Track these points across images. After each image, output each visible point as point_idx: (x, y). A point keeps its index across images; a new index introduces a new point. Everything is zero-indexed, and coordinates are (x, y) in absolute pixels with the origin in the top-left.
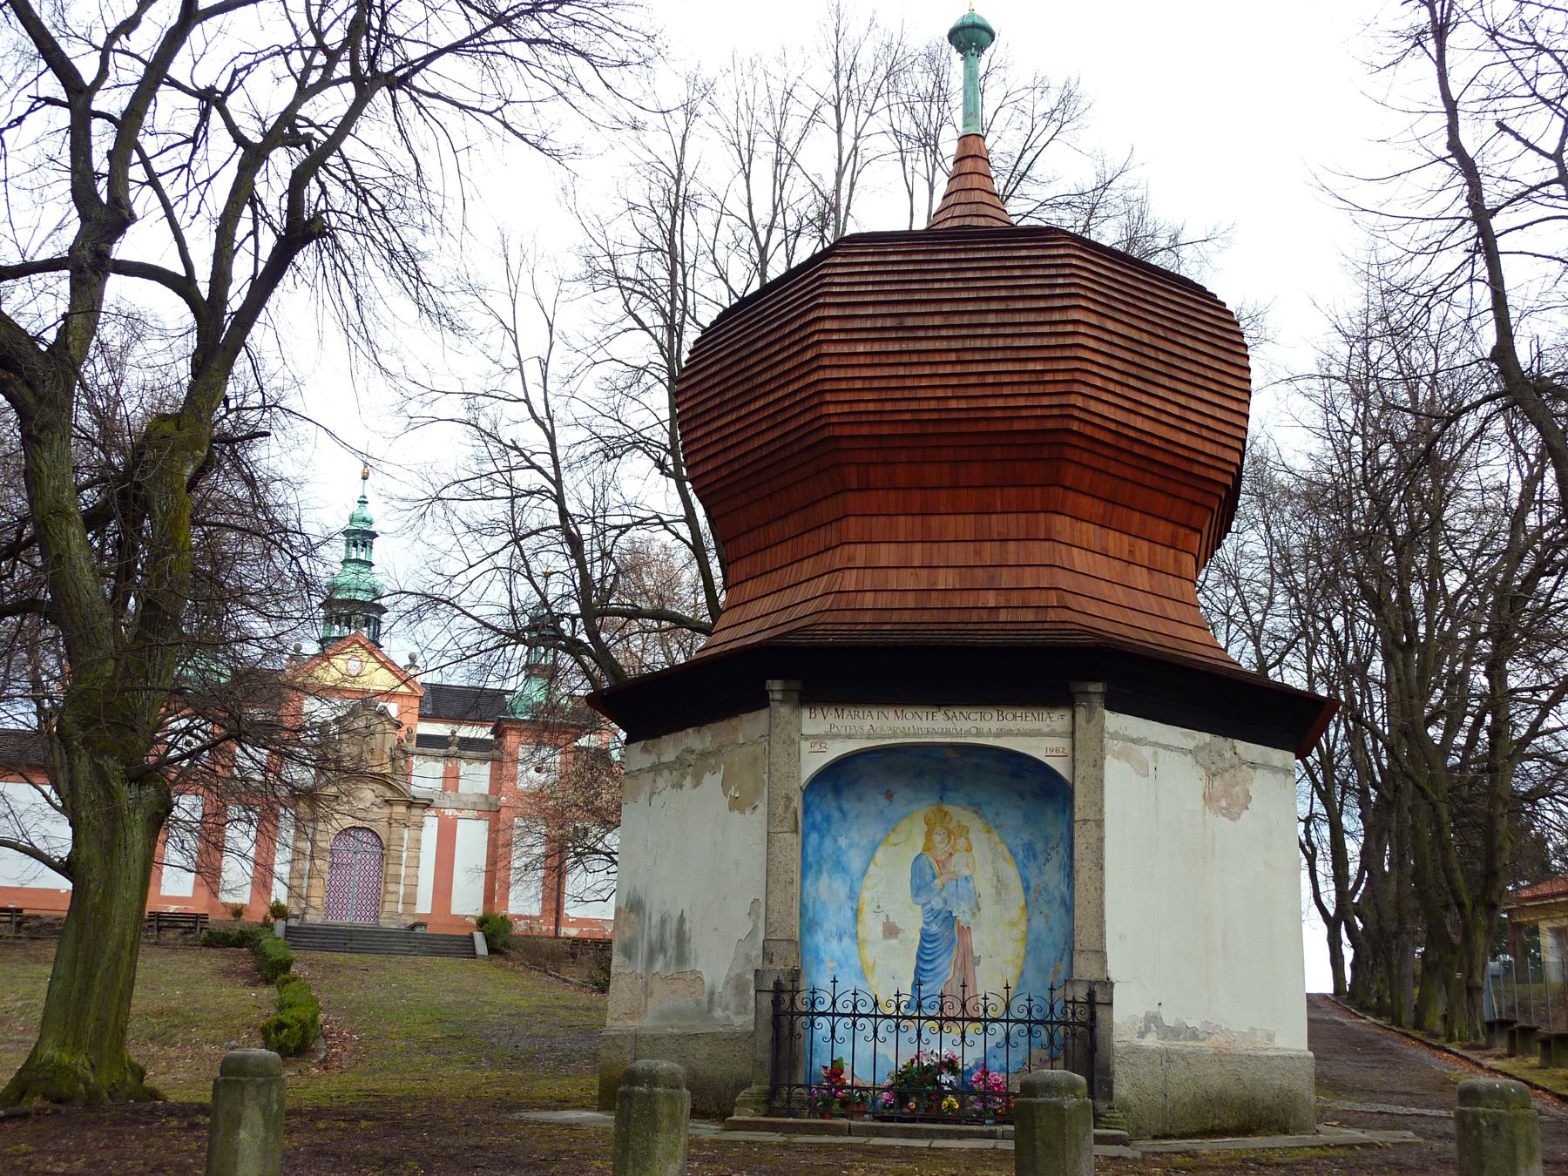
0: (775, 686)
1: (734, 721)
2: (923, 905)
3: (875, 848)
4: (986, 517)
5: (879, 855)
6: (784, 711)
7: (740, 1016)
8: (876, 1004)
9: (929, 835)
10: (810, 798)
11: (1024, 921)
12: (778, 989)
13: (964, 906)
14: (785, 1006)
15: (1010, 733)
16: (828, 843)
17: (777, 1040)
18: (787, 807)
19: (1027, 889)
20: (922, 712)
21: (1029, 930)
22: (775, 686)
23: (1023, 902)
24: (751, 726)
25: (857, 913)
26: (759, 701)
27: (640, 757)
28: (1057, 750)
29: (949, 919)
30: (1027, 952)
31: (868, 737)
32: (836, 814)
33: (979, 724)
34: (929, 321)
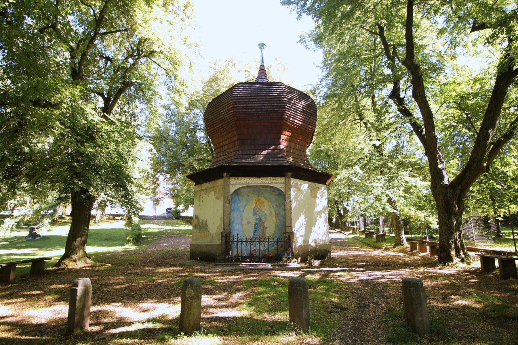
0: (225, 174)
3: (245, 206)
5: (246, 207)
6: (227, 179)
7: (218, 241)
9: (256, 204)
12: (226, 235)
14: (227, 237)
15: (272, 183)
16: (236, 206)
17: (226, 246)
19: (276, 214)
20: (255, 178)
22: (225, 174)
24: (220, 182)
25: (242, 219)
26: (222, 177)
27: (198, 188)
29: (260, 220)
32: (237, 199)
34: (255, 100)
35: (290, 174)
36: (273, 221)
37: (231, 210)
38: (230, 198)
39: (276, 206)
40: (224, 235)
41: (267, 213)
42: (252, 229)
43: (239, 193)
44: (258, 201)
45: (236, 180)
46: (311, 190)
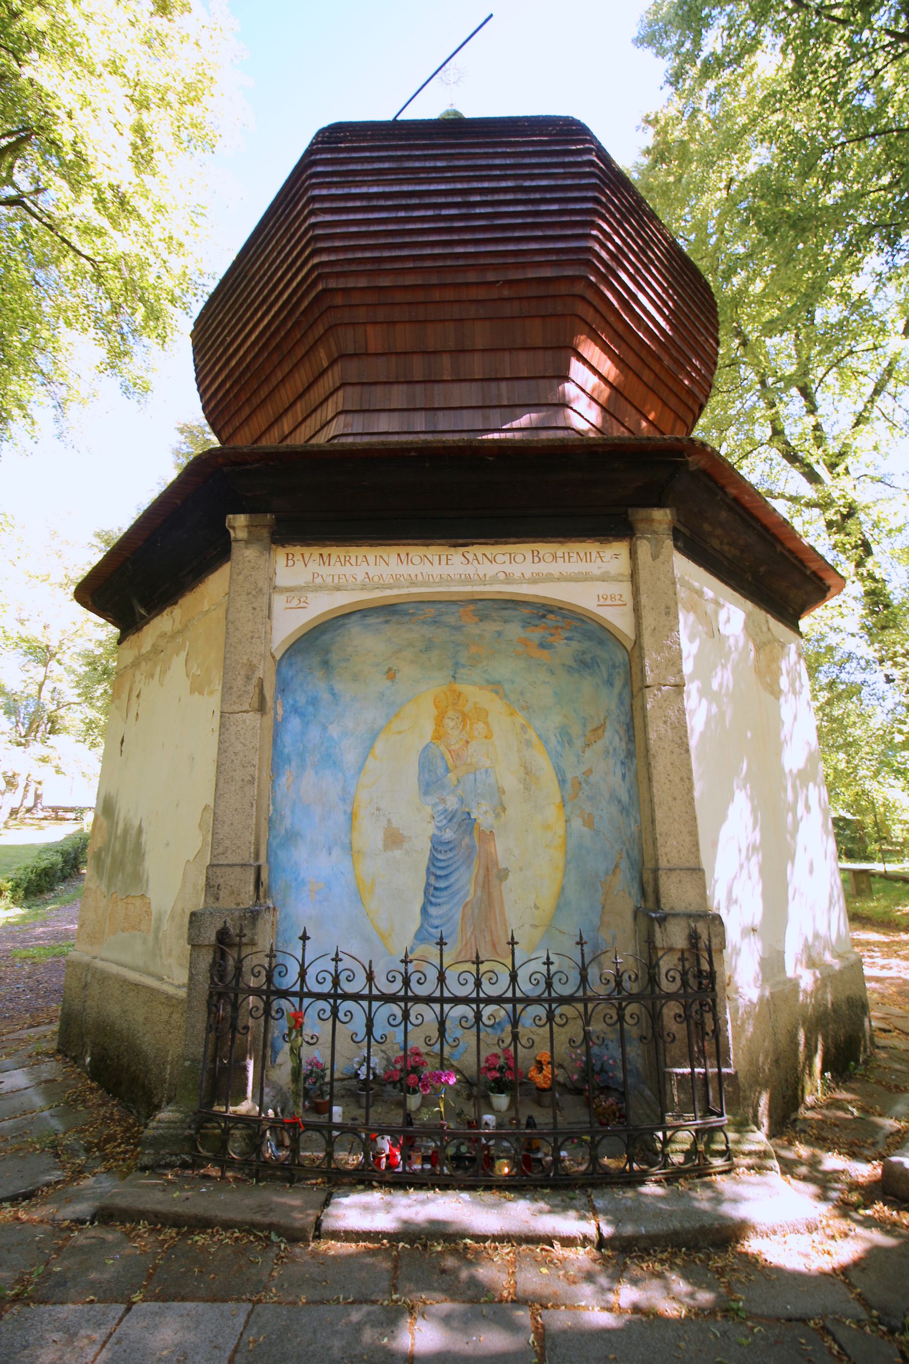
0: (238, 523)
1: (141, 512)
2: (435, 805)
3: (374, 736)
4: (493, 385)
5: (379, 746)
7: (172, 969)
8: (370, 977)
9: (439, 721)
10: (289, 673)
11: (562, 824)
13: (485, 806)
15: (549, 578)
16: (314, 733)
18: (248, 678)
19: (562, 782)
20: (434, 552)
21: (568, 834)
22: (238, 523)
23: (558, 799)
25: (352, 817)
28: (612, 598)
29: (467, 822)
30: (567, 863)
31: (363, 588)
32: (325, 696)
33: (508, 568)
35: (662, 516)
36: (547, 827)
37: (277, 761)
38: (266, 671)
39: (565, 736)
40: (210, 936)
41: (510, 781)
42: (413, 882)
43: (334, 658)
44: (451, 707)
45: (314, 566)
46: (758, 649)
